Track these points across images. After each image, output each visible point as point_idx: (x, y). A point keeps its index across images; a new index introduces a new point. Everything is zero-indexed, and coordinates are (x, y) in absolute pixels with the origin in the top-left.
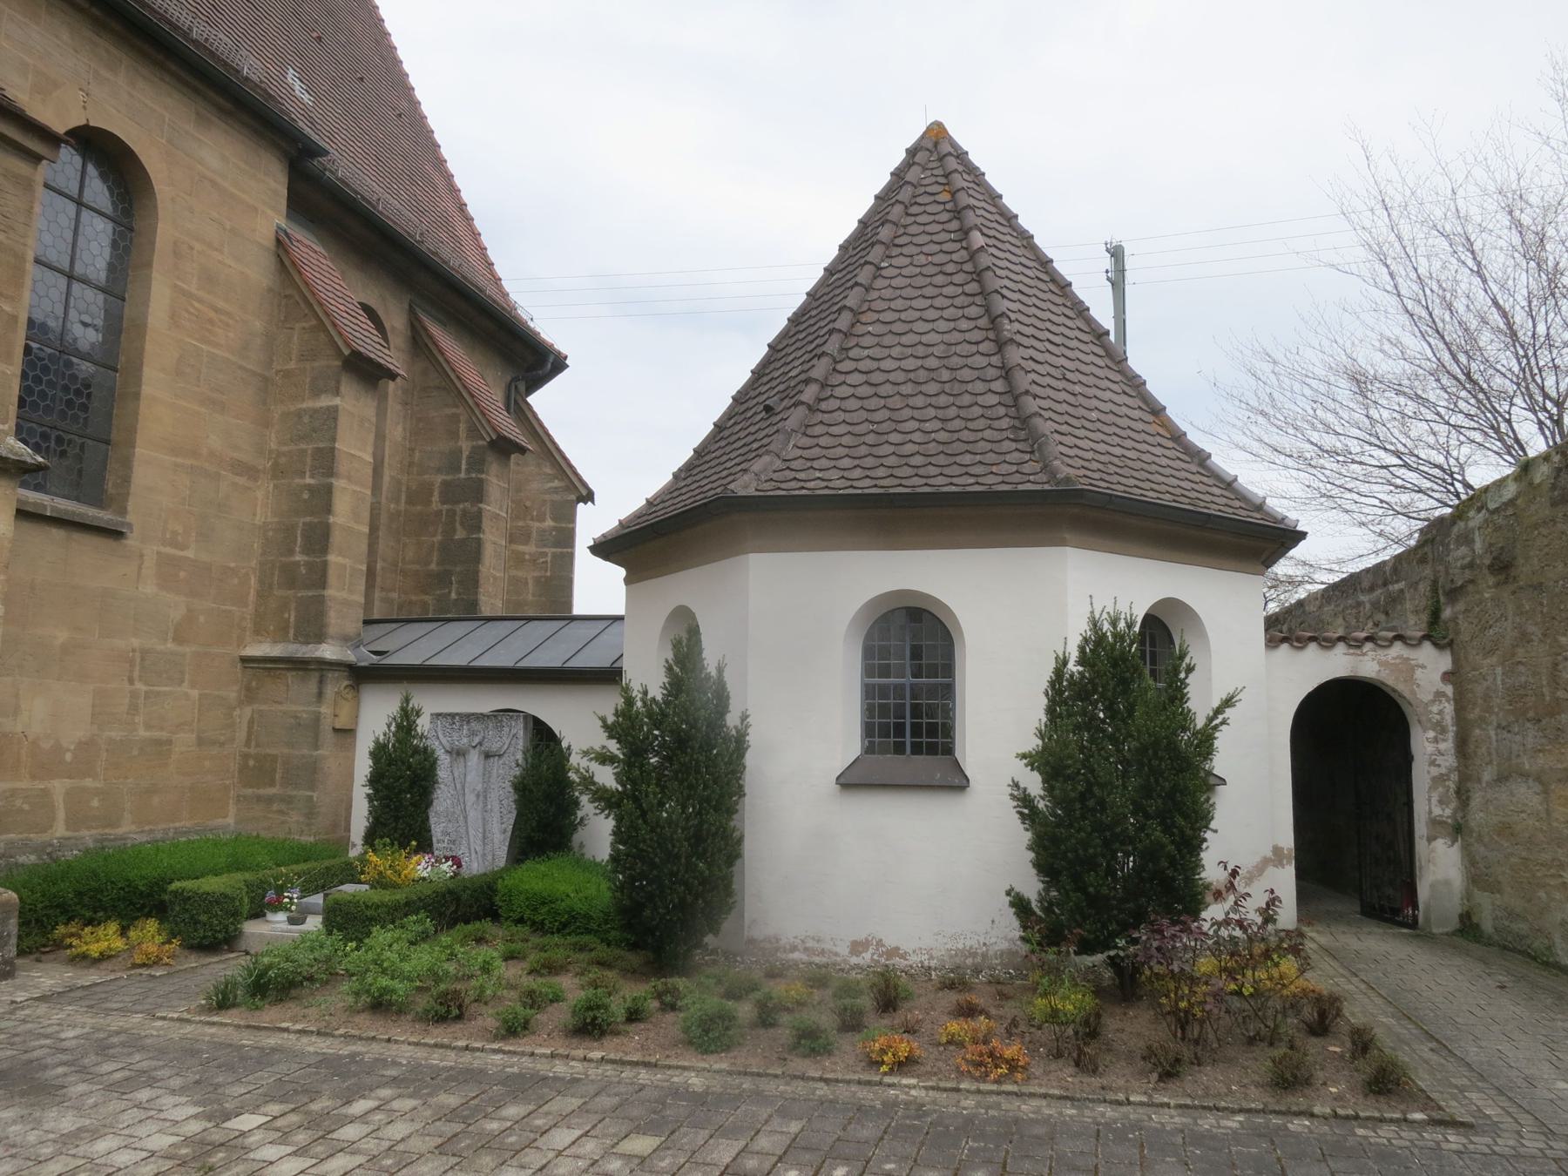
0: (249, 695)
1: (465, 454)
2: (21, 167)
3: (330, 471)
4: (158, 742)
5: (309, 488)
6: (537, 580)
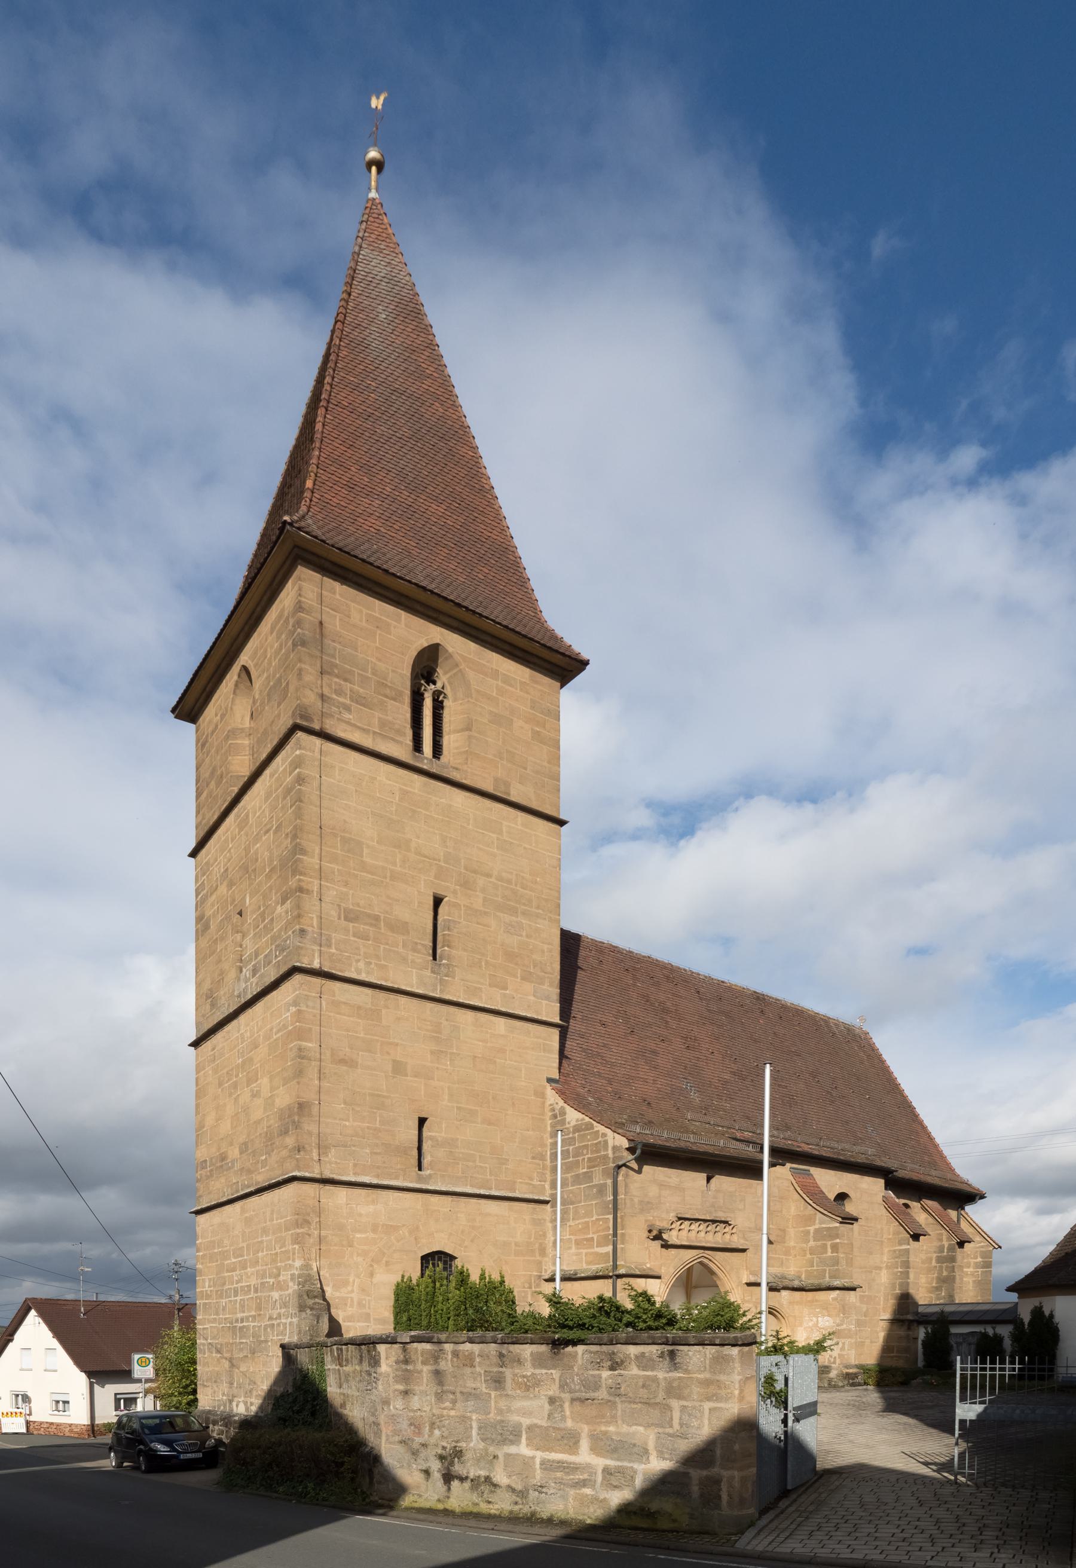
0: (361, 1419)
1: (946, 1246)
2: (850, 1226)
3: (908, 1267)
4: (862, 1342)
5: (901, 1272)
6: (974, 1282)
